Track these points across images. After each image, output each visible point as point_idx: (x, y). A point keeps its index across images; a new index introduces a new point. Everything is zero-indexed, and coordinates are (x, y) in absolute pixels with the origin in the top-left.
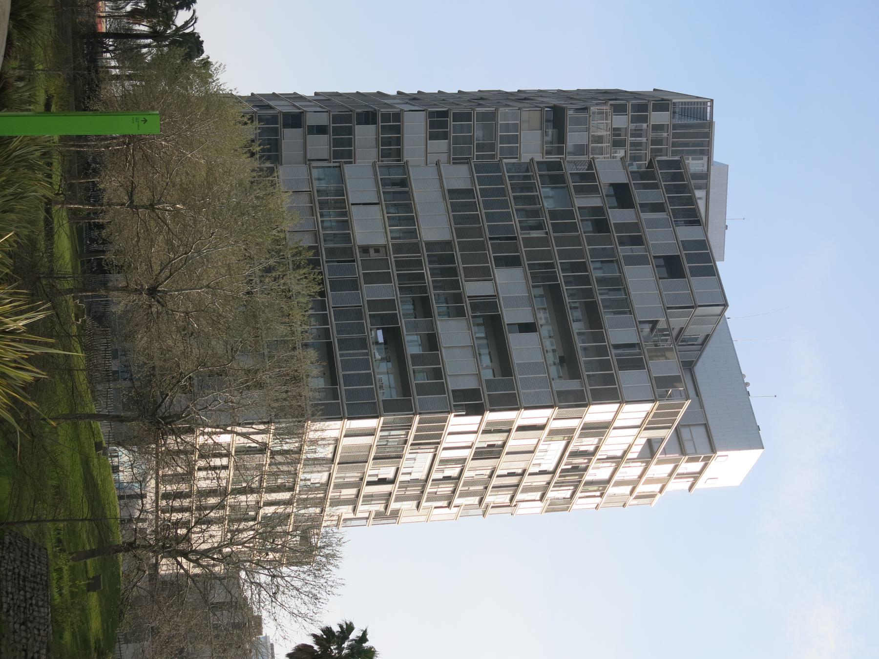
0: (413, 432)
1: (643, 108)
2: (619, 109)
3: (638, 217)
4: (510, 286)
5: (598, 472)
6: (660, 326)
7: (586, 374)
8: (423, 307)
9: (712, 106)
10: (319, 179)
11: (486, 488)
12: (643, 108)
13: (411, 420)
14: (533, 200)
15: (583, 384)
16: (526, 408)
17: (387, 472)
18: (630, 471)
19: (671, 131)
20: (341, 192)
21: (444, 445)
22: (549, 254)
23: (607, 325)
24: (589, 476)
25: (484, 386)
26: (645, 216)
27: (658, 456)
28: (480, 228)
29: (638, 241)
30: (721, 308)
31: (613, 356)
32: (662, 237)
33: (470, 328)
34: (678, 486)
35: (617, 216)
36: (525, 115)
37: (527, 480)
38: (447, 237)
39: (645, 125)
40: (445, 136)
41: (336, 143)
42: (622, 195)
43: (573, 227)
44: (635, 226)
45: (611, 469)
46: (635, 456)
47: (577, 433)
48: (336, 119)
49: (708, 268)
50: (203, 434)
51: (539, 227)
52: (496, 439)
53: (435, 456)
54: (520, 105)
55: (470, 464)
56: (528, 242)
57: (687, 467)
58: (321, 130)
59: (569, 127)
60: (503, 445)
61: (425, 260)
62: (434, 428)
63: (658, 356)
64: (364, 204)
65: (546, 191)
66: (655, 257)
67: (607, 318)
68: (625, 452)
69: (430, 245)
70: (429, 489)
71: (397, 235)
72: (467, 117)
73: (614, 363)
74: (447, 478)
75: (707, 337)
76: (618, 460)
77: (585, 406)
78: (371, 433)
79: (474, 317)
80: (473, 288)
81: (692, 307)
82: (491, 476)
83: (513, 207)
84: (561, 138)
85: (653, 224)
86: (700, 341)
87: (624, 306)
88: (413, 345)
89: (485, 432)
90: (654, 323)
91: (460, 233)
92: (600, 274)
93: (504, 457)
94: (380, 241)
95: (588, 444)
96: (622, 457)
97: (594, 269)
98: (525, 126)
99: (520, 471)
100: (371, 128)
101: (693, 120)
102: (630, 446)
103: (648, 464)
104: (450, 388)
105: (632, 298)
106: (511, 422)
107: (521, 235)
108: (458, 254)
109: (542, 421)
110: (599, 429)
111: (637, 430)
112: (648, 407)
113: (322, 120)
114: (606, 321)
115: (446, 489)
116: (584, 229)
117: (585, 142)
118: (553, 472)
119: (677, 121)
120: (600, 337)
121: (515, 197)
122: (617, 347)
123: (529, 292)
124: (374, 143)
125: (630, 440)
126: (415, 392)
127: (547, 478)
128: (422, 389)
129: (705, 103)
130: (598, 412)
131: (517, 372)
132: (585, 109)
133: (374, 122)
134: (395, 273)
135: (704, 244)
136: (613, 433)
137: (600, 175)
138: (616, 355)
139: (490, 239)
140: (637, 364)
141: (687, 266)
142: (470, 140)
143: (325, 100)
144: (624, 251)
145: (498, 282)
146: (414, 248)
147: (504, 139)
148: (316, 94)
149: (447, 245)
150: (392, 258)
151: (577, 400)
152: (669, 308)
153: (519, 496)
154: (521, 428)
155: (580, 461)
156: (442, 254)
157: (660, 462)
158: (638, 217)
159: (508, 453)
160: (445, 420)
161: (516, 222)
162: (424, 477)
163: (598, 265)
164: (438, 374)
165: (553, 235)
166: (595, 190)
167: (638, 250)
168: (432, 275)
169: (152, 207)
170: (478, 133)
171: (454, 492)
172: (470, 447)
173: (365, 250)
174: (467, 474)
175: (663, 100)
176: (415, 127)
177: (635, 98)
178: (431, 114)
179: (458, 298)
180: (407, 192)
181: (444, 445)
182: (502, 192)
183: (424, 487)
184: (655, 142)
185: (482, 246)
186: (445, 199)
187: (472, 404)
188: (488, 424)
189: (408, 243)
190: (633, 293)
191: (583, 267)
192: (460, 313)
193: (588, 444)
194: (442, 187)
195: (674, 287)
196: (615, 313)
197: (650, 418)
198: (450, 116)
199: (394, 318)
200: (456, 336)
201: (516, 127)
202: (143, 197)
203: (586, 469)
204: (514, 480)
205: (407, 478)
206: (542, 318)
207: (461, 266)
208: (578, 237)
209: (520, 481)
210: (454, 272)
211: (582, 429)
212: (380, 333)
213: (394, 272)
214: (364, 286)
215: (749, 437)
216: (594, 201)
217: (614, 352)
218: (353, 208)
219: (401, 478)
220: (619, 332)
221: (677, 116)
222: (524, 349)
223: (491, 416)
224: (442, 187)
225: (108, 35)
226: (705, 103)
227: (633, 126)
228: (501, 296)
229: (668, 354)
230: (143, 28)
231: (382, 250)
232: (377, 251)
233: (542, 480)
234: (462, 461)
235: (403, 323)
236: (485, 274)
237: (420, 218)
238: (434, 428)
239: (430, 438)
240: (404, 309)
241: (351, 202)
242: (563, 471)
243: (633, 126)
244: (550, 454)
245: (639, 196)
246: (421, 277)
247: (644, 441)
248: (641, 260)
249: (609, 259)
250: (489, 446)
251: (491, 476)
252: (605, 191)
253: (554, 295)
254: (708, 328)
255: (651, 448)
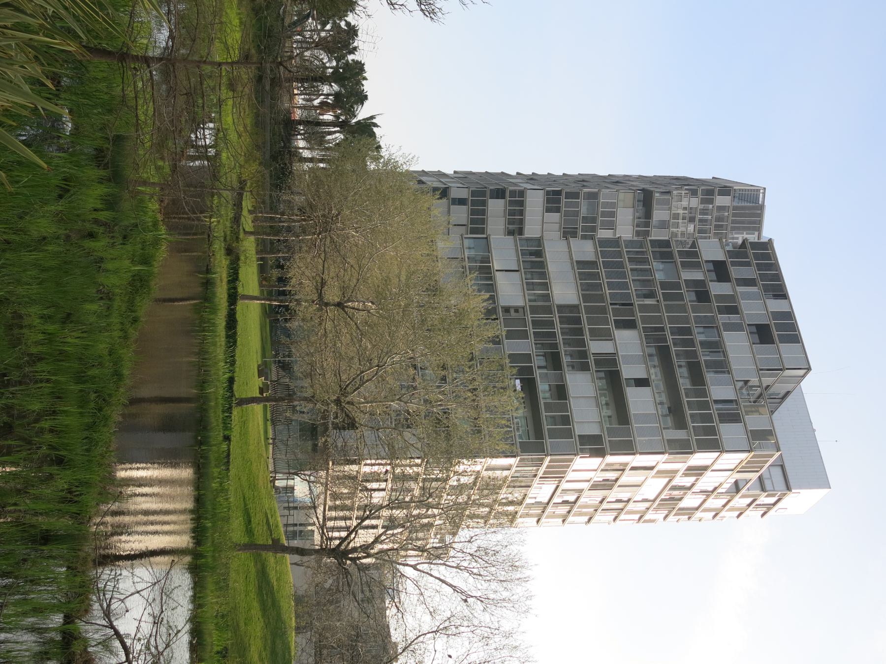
0: (543, 469)
1: (710, 192)
2: (694, 193)
3: (734, 290)
4: (627, 345)
5: (690, 501)
6: (750, 384)
7: (694, 423)
8: (554, 361)
9: (764, 193)
10: (469, 248)
11: (596, 510)
12: (710, 192)
13: (542, 460)
14: (649, 272)
15: (689, 434)
16: (641, 453)
17: (517, 495)
18: (715, 503)
19: (731, 211)
20: (487, 259)
21: (567, 478)
22: (659, 319)
23: (709, 382)
24: (683, 504)
25: (606, 433)
26: (741, 289)
27: (743, 491)
28: (602, 295)
29: (734, 310)
30: (804, 371)
31: (714, 410)
32: (755, 307)
33: (593, 381)
34: (753, 514)
35: (717, 289)
36: (621, 196)
37: (631, 506)
38: (576, 302)
39: (711, 206)
40: (557, 210)
41: (473, 212)
42: (720, 270)
43: (680, 297)
44: (732, 298)
45: (701, 500)
46: (724, 491)
47: (680, 473)
48: (474, 194)
49: (793, 336)
50: (365, 465)
51: (651, 295)
52: (612, 475)
53: (557, 487)
54: (617, 188)
55: (586, 493)
56: (643, 308)
57: (764, 499)
58: (461, 202)
59: (655, 206)
60: (617, 480)
61: (557, 320)
62: (563, 467)
63: (752, 412)
64: (506, 271)
65: (656, 265)
66: (749, 325)
67: (709, 376)
68: (715, 489)
69: (561, 308)
70: (549, 509)
71: (533, 298)
72: (576, 195)
73: (716, 417)
74: (565, 502)
75: (788, 393)
76: (708, 493)
77: (691, 453)
78: (508, 468)
79: (597, 371)
80: (596, 347)
81: (781, 370)
82: (601, 502)
83: (630, 277)
84: (648, 214)
85: (748, 296)
86: (780, 396)
87: (722, 366)
88: (543, 388)
89: (602, 470)
90: (746, 382)
91: (586, 298)
92: (702, 338)
93: (615, 489)
94: (520, 303)
95: (688, 481)
96: (713, 492)
97: (698, 333)
98: (621, 204)
99: (626, 499)
100: (501, 202)
101: (748, 204)
102: (721, 484)
103: (733, 497)
104: (577, 433)
105: (730, 360)
106: (626, 464)
107: (637, 302)
108: (584, 317)
109: (653, 464)
110: (699, 471)
111: (730, 472)
112: (743, 456)
113: (464, 194)
114: (708, 379)
115: (564, 510)
116: (689, 297)
117: (667, 218)
118: (654, 501)
119: (735, 204)
120: (704, 393)
121: (632, 270)
122: (716, 402)
123: (643, 351)
124: (502, 214)
125: (722, 480)
126: (543, 432)
127: (647, 505)
128: (553, 434)
129: (758, 191)
130: (700, 458)
131: (633, 421)
132: (669, 192)
133: (503, 197)
134: (532, 331)
135: (789, 315)
136: (708, 473)
137: (702, 252)
138: (717, 409)
139: (611, 304)
140: (734, 418)
141: (775, 333)
142: (577, 214)
143: (464, 177)
144: (723, 318)
145: (618, 342)
146: (548, 310)
147: (604, 214)
148: (455, 172)
149: (574, 308)
150: (529, 317)
151: (683, 448)
152: (761, 370)
153: (622, 516)
154: (633, 468)
155: (676, 493)
156: (570, 315)
157: (743, 496)
158: (734, 290)
159: (619, 486)
160: (571, 461)
161: (633, 289)
162: (546, 501)
163: (701, 330)
164: (566, 420)
165: (663, 303)
166: (697, 266)
167: (734, 318)
168: (562, 334)
169: (339, 305)
170: (584, 210)
171: (569, 512)
172: (588, 481)
173: (507, 310)
174: (582, 500)
175: (725, 187)
176: (535, 202)
177: (703, 185)
178: (548, 193)
179: (584, 354)
180: (542, 262)
181: (567, 478)
182: (621, 265)
183: (545, 508)
184: (719, 219)
185: (603, 310)
186: (573, 268)
187: (594, 446)
188: (607, 465)
189: (543, 303)
190: (731, 355)
191: (688, 331)
192: (585, 367)
193: (688, 481)
194: (571, 259)
195: (765, 352)
196: (716, 372)
197: (743, 464)
198: (569, 197)
199: (530, 370)
200: (582, 387)
201: (613, 205)
202: (332, 295)
203: (681, 499)
204: (620, 506)
205: (533, 501)
206: (656, 375)
207: (587, 327)
208: (684, 305)
209: (625, 506)
210: (580, 332)
211: (686, 470)
212: (518, 382)
213: (531, 330)
214: (506, 341)
215: (820, 480)
216: (698, 275)
217: (715, 406)
218: (497, 273)
219: (528, 501)
220: (719, 390)
221: (736, 200)
222: (640, 402)
223: (610, 459)
224: (571, 259)
225: (300, 122)
226: (758, 191)
227: (701, 206)
228: (620, 354)
229: (761, 409)
230: (328, 117)
231: (521, 310)
232: (516, 311)
233: (643, 506)
234: (581, 491)
235: (538, 373)
236: (606, 336)
237: (553, 284)
238: (563, 467)
239: (557, 474)
240: (538, 361)
241: (496, 268)
242: (662, 500)
243: (701, 206)
244: (653, 487)
245: (735, 272)
246: (553, 335)
247: (734, 480)
248: (737, 327)
249: (710, 325)
250: (604, 480)
251: (601, 502)
252: (705, 267)
253: (664, 354)
254: (789, 387)
255: (737, 487)
